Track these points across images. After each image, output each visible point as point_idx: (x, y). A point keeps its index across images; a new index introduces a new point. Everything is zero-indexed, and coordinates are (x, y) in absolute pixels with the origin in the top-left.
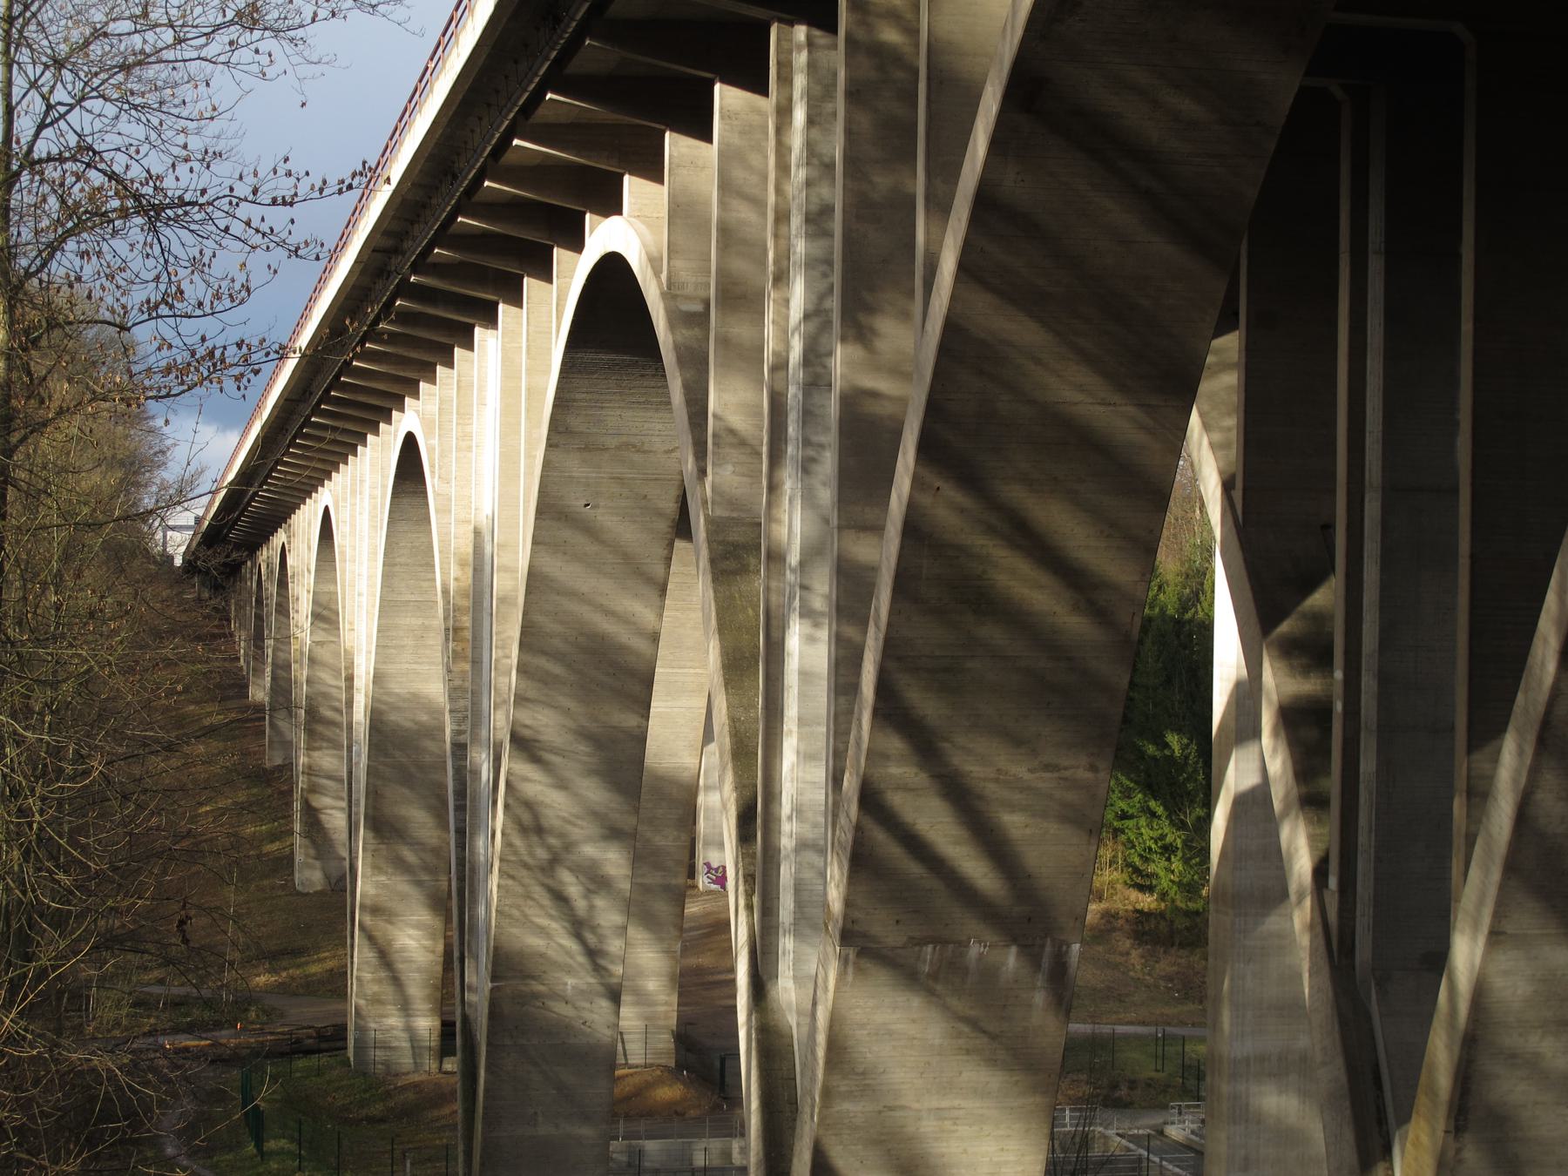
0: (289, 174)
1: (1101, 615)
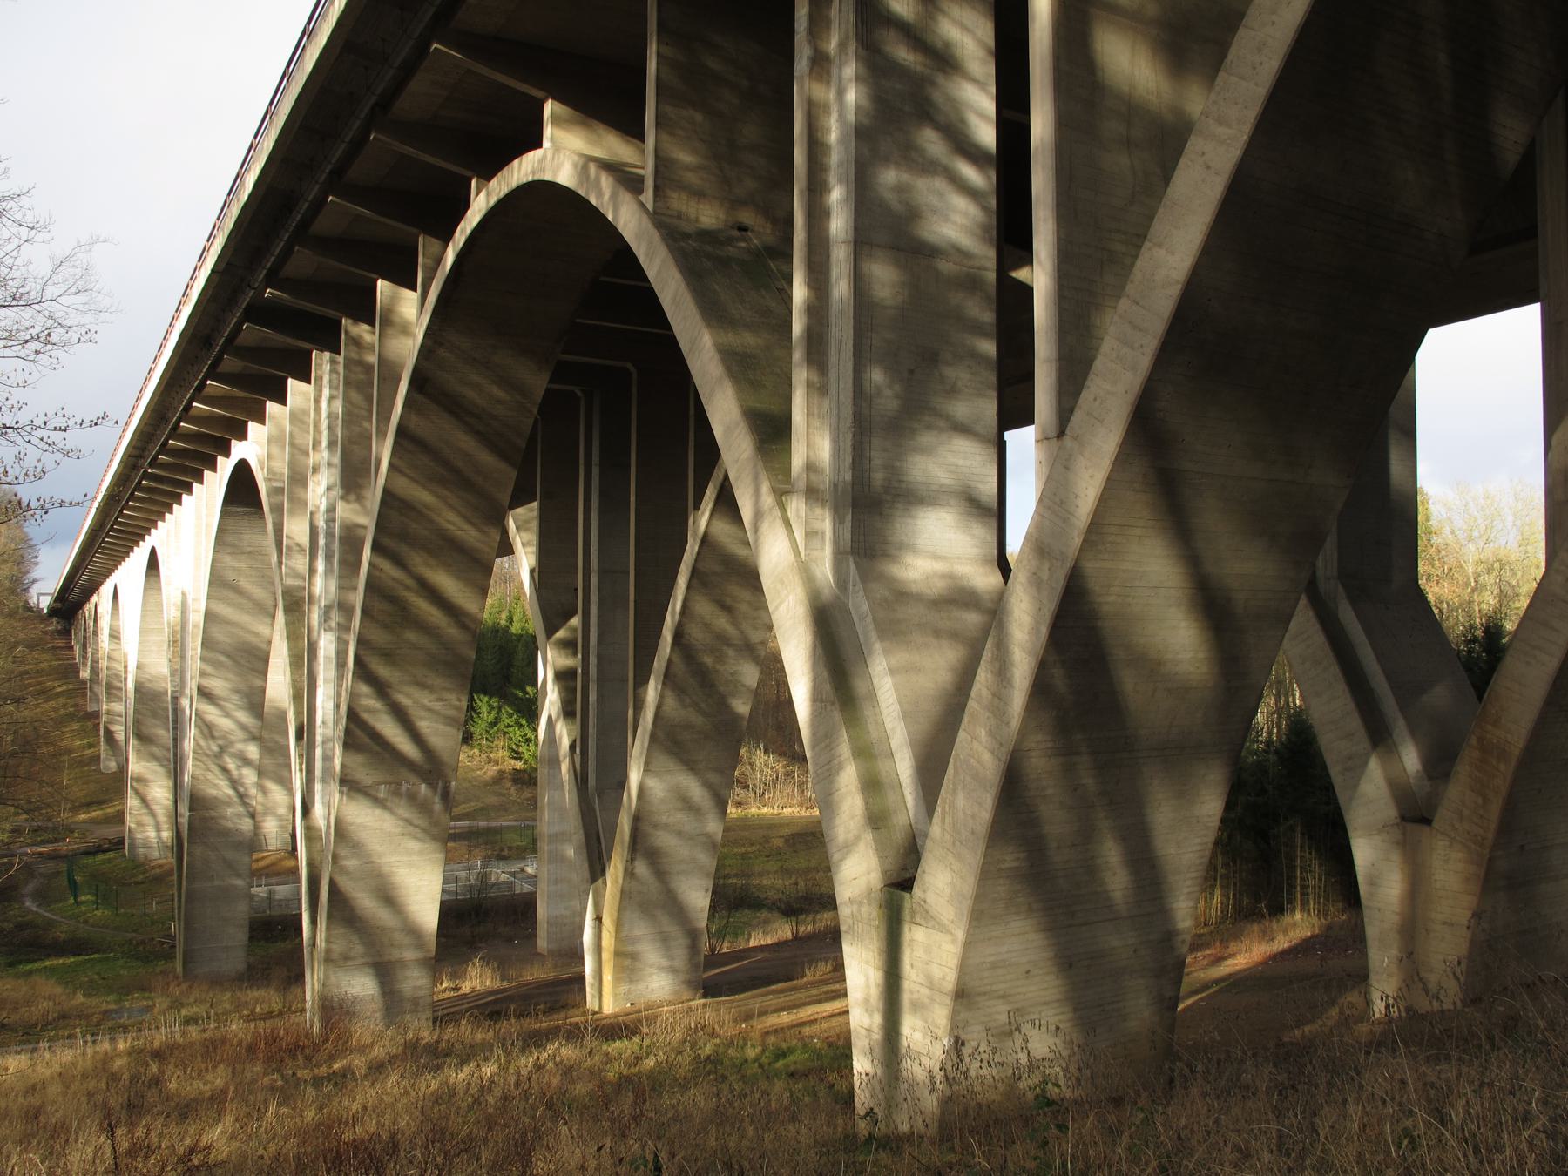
0: (64, 416)
1: (463, 626)
